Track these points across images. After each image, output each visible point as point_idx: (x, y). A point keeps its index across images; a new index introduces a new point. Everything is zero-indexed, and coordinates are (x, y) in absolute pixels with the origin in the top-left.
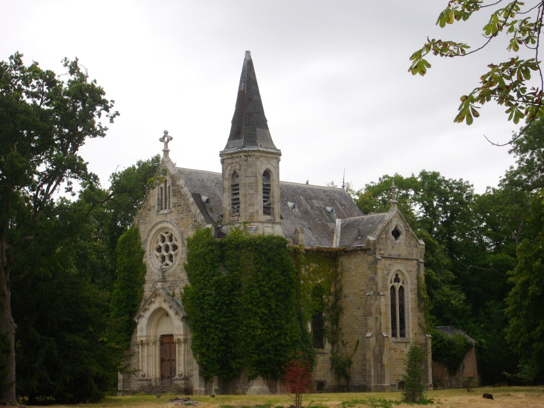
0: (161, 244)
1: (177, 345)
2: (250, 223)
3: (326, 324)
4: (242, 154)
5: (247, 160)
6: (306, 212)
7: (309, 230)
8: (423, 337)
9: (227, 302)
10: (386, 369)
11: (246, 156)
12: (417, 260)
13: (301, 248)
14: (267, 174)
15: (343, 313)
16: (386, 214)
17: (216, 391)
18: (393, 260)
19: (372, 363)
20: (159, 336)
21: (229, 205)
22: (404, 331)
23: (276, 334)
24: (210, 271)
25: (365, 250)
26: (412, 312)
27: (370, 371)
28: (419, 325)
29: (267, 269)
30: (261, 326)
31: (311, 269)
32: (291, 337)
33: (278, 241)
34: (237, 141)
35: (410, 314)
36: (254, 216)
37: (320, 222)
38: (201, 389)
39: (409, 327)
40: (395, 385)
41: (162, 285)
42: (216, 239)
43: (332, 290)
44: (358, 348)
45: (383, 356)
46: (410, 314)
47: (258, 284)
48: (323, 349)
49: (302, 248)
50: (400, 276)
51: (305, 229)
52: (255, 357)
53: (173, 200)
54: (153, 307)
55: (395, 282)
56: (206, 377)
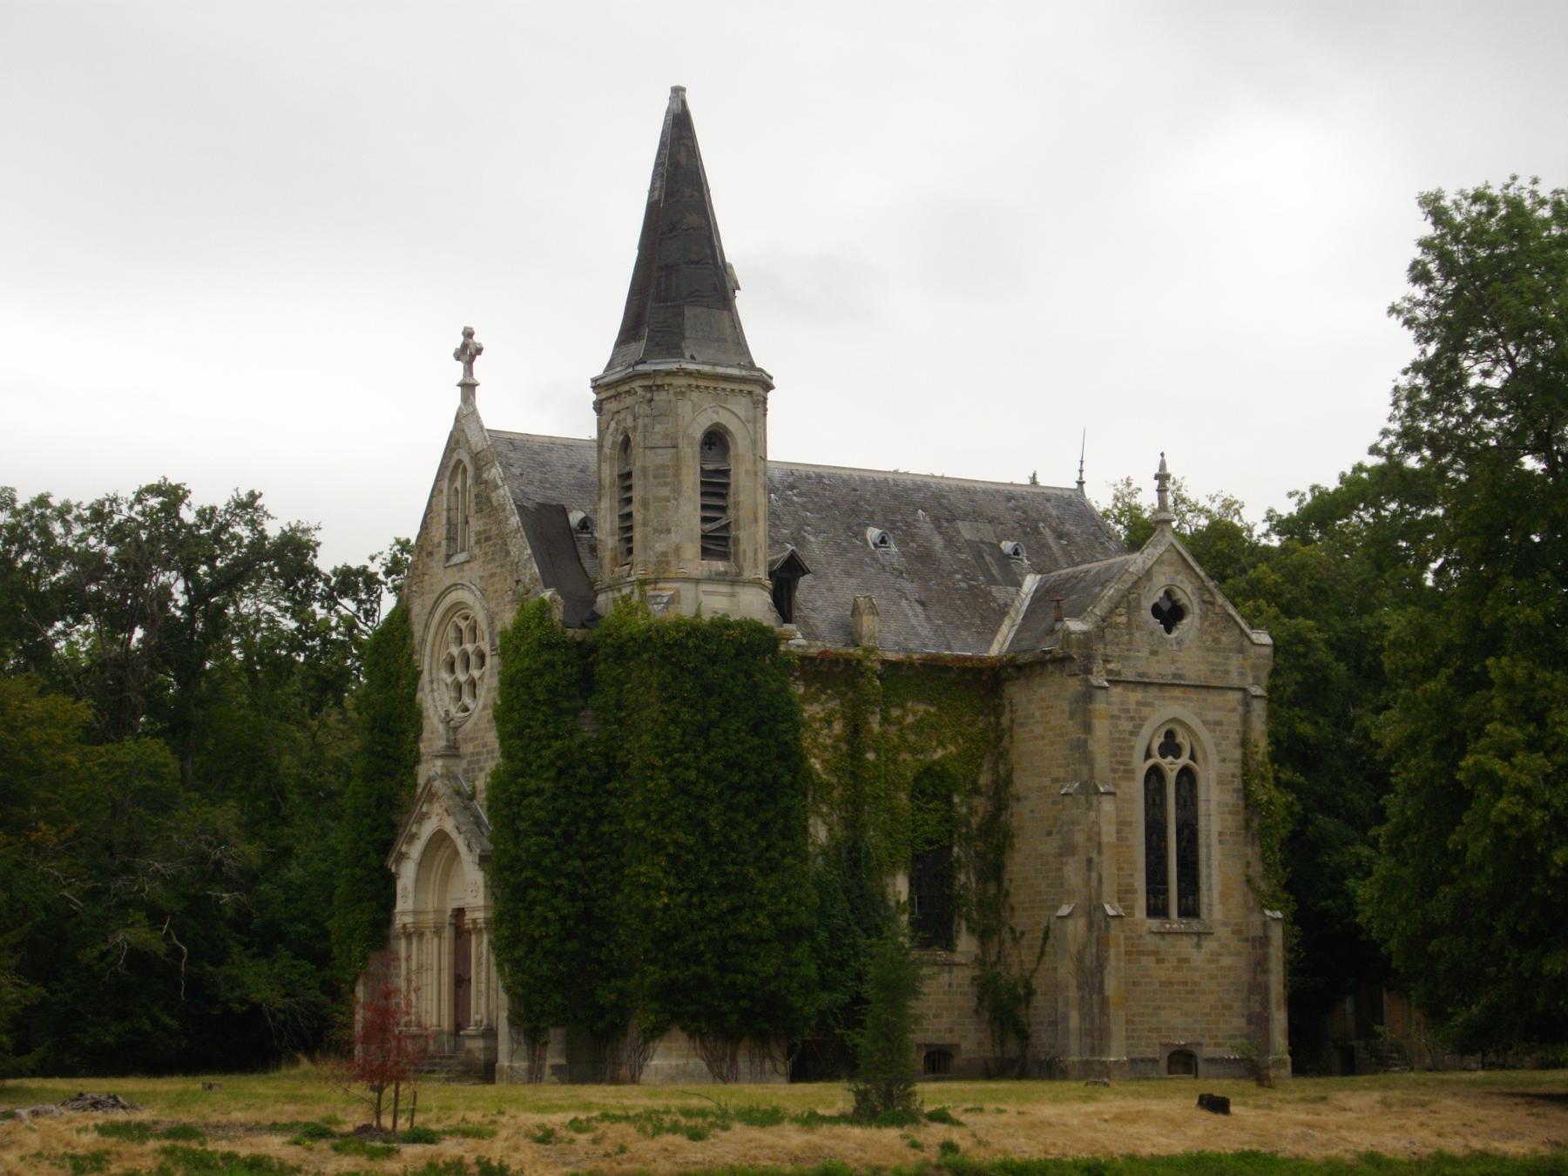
0: (455, 651)
1: (473, 937)
2: (656, 581)
3: (963, 878)
4: (636, 385)
5: (651, 400)
6: (923, 558)
7: (919, 609)
8: (1256, 919)
9: (591, 813)
10: (1112, 1010)
11: (648, 388)
12: (1243, 690)
13: (867, 658)
14: (716, 440)
15: (1012, 846)
16: (1137, 555)
17: (557, 1069)
18: (1154, 691)
19: (1073, 994)
20: (449, 912)
21: (612, 534)
22: (1197, 903)
23: (725, 905)
24: (545, 723)
25: (1062, 661)
26: (1220, 842)
27: (1066, 1018)
28: (1249, 881)
29: (699, 717)
30: (672, 881)
31: (910, 719)
32: (774, 918)
33: (743, 634)
34: (633, 346)
35: (1216, 851)
36: (668, 563)
37: (964, 585)
38: (516, 1065)
39: (1210, 889)
40: (1154, 1061)
41: (445, 767)
42: (570, 632)
43: (984, 779)
44: (1047, 949)
45: (1106, 972)
46: (1216, 851)
47: (668, 760)
48: (952, 951)
49: (873, 657)
50: (1182, 738)
51: (904, 603)
52: (654, 973)
54: (427, 830)
55: (1163, 756)
56: (530, 1024)
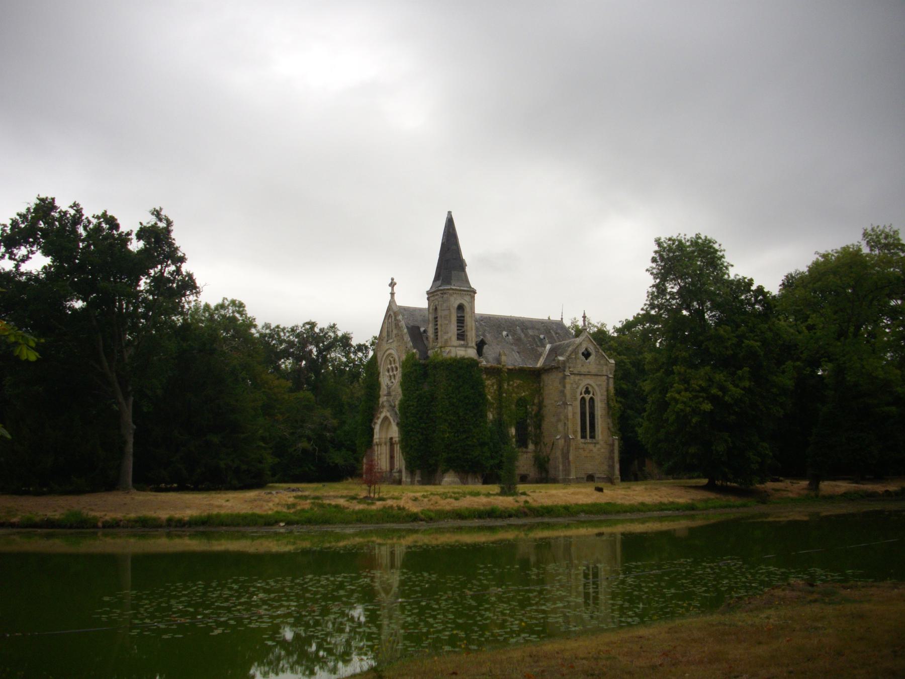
8: (611, 439)
14: (461, 308)
19: (560, 460)
25: (557, 368)
43: (536, 401)
50: (590, 389)
53: (395, 332)
54: (382, 416)
56: (411, 469)
